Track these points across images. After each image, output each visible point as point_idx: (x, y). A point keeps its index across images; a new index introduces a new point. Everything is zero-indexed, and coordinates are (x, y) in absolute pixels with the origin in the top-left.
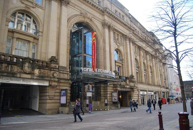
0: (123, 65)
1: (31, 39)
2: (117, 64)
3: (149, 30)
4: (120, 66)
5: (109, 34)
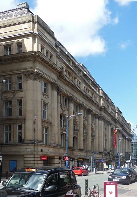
0: (77, 135)
2: (45, 124)
3: (128, 123)
4: (64, 134)
5: (103, 123)
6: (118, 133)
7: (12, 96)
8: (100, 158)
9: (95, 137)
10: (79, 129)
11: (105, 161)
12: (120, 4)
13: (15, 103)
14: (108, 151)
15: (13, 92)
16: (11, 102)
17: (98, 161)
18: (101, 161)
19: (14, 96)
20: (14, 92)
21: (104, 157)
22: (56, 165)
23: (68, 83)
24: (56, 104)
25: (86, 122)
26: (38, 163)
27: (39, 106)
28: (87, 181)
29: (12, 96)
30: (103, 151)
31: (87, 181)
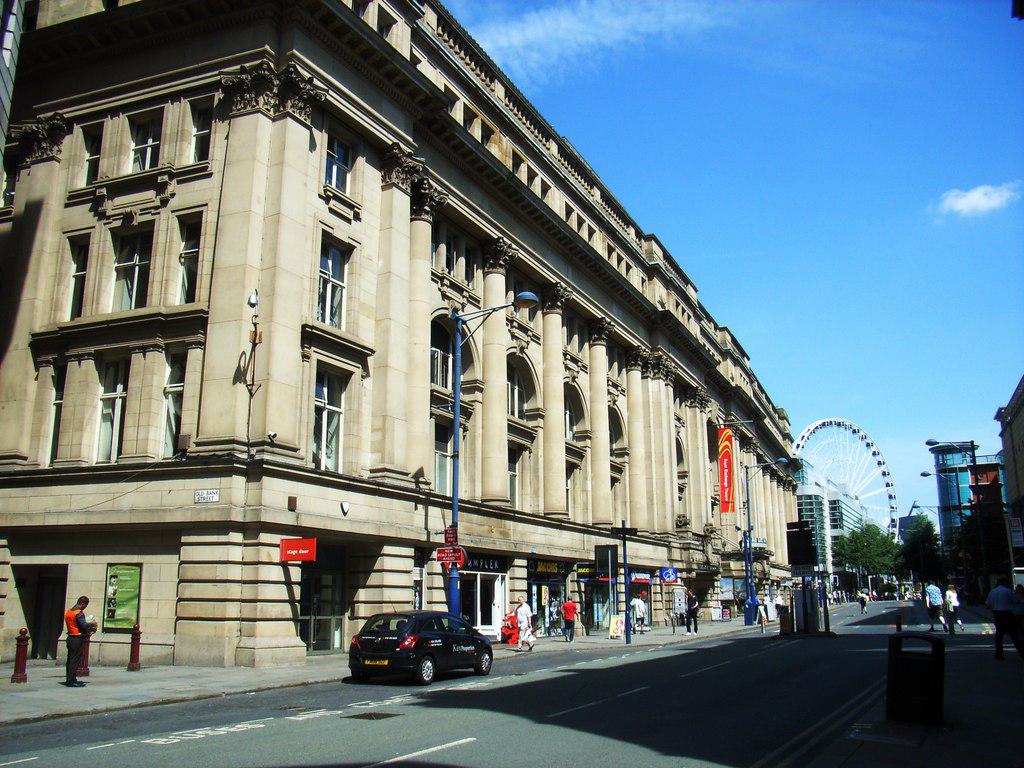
4: (523, 448)
6: (736, 444)
7: (158, 203)
8: (660, 560)
10: (544, 410)
11: (684, 575)
12: (956, 191)
13: (168, 239)
14: (696, 527)
15: (160, 180)
16: (147, 231)
17: (647, 576)
18: (661, 577)
19: (164, 203)
20: (166, 178)
21: (676, 554)
22: (389, 595)
23: (530, 213)
24: (405, 258)
25: (622, 402)
26: (262, 577)
27: (303, 258)
28: (6, 580)
29: (158, 203)
30: (670, 526)
31: (6, 580)
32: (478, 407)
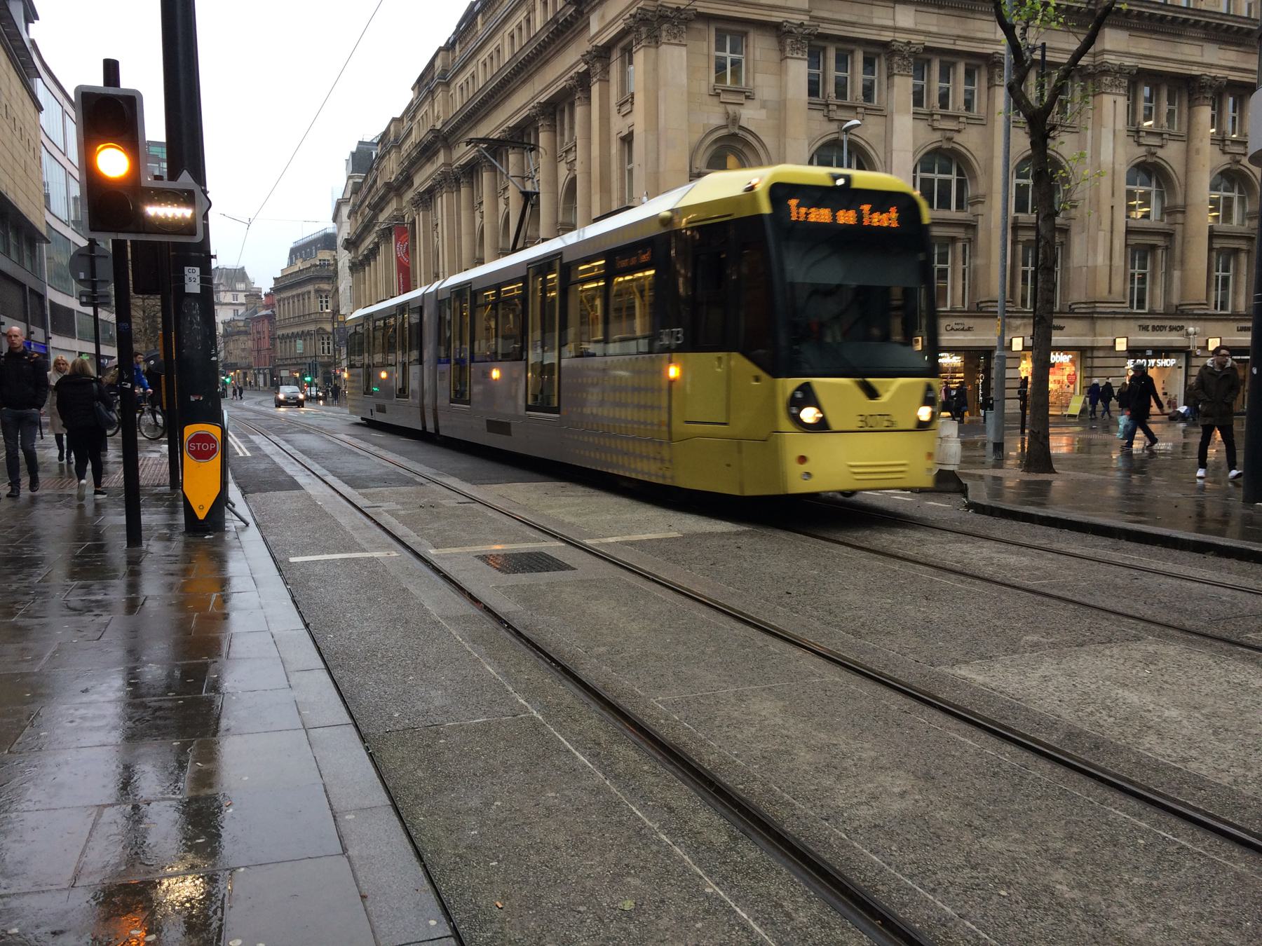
1: (959, 233)
9: (1183, 212)
32: (1179, 228)
